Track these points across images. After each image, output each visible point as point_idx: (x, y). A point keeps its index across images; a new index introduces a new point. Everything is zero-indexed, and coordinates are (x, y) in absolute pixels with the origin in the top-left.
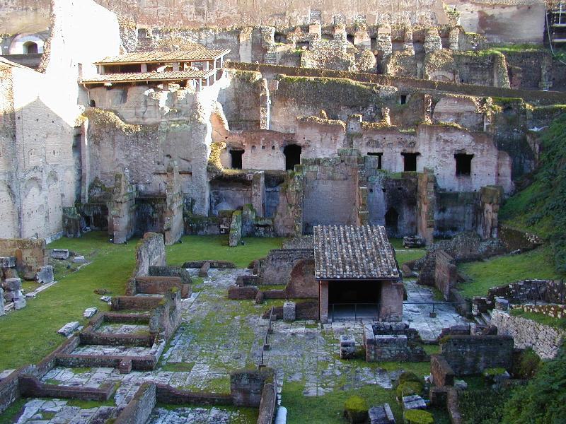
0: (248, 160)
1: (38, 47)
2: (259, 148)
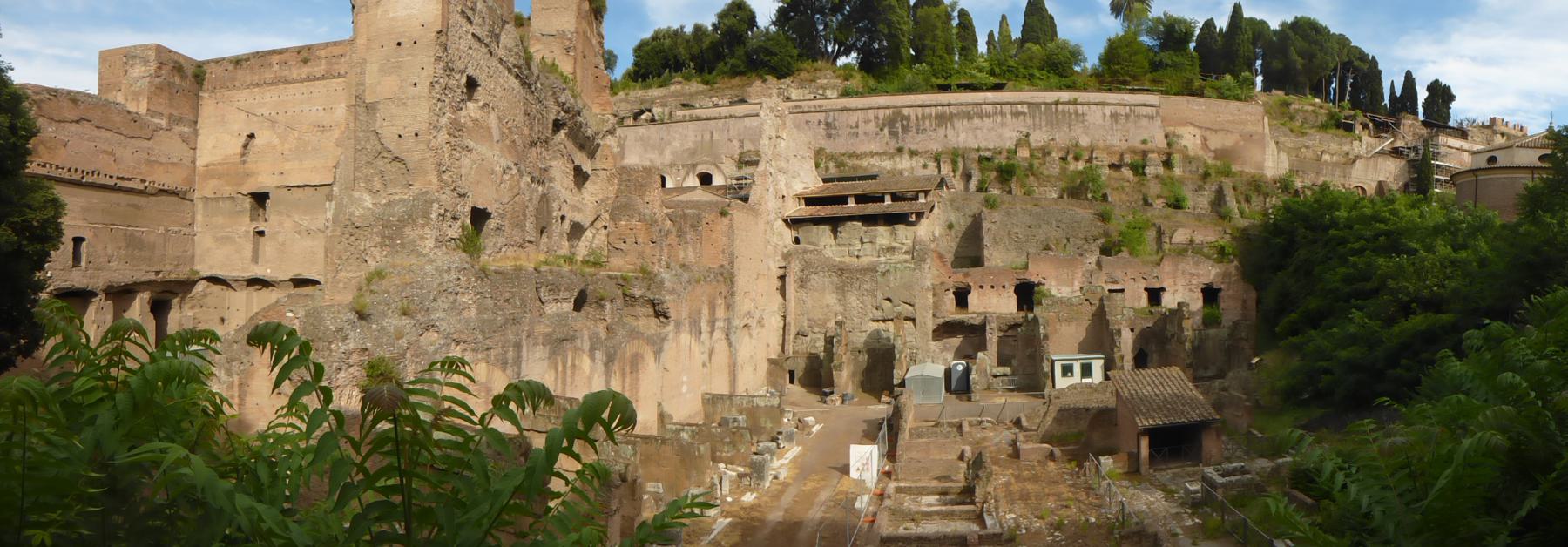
0: (973, 299)
1: (1323, 19)
2: (987, 287)
